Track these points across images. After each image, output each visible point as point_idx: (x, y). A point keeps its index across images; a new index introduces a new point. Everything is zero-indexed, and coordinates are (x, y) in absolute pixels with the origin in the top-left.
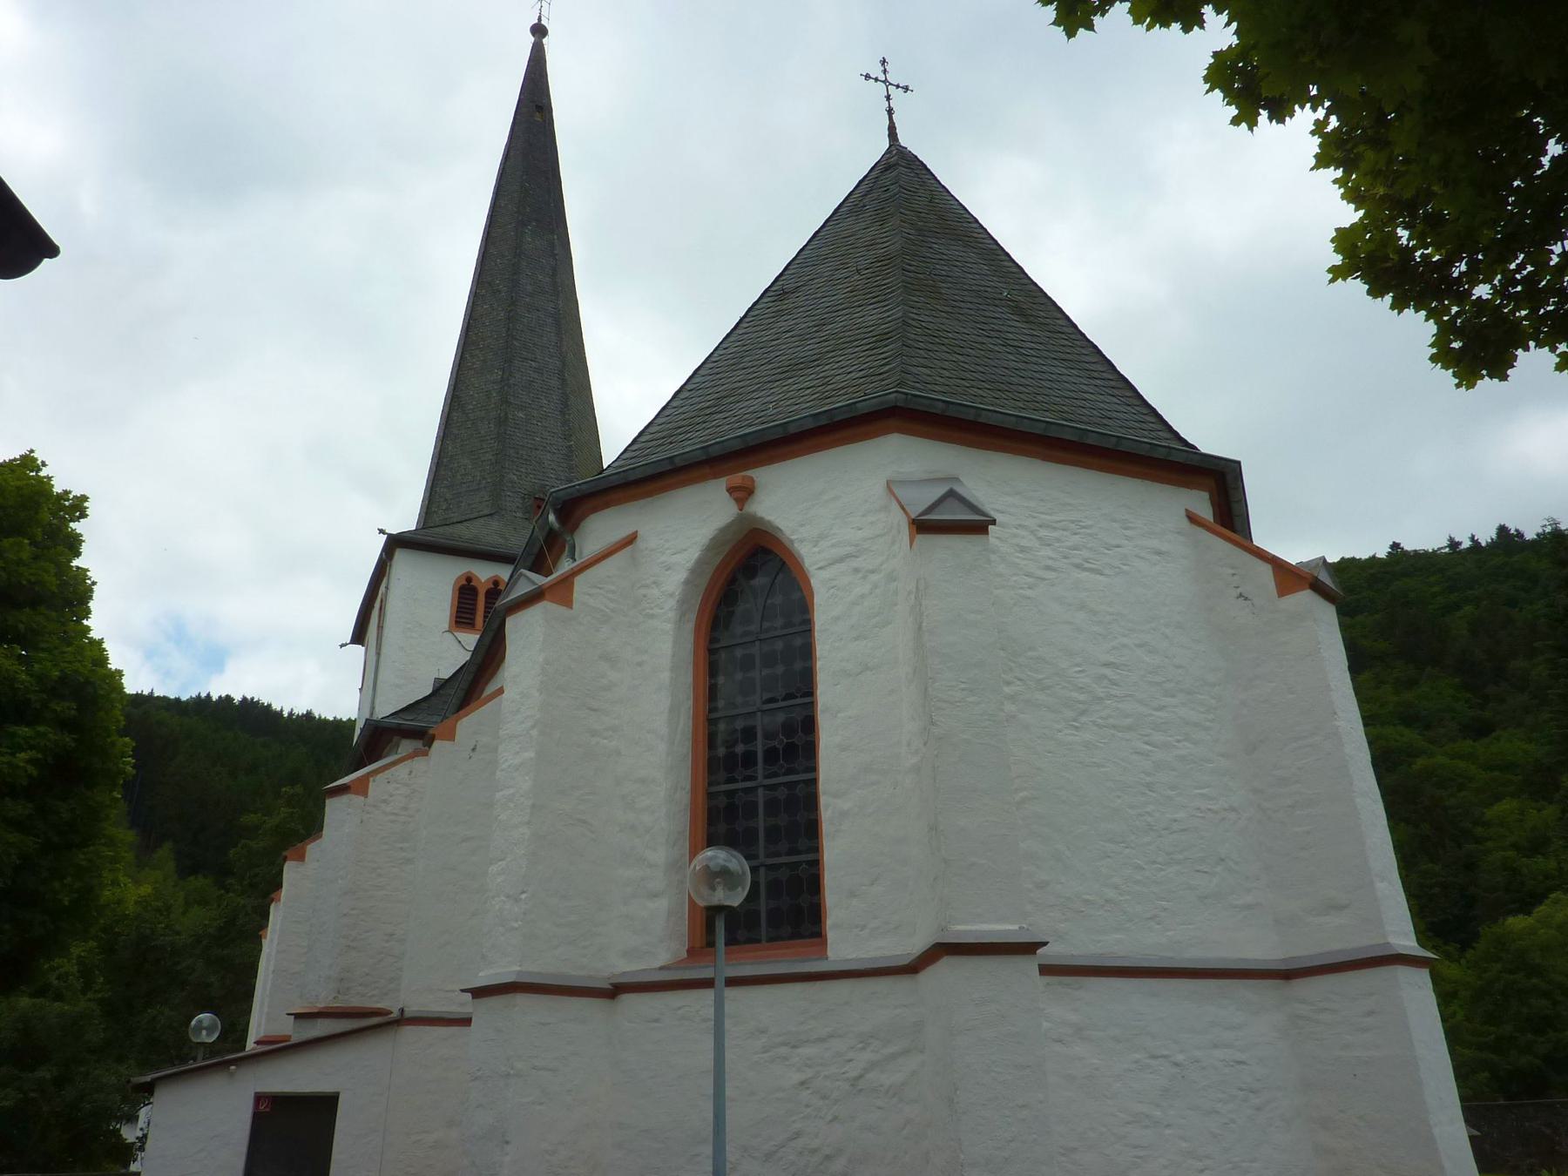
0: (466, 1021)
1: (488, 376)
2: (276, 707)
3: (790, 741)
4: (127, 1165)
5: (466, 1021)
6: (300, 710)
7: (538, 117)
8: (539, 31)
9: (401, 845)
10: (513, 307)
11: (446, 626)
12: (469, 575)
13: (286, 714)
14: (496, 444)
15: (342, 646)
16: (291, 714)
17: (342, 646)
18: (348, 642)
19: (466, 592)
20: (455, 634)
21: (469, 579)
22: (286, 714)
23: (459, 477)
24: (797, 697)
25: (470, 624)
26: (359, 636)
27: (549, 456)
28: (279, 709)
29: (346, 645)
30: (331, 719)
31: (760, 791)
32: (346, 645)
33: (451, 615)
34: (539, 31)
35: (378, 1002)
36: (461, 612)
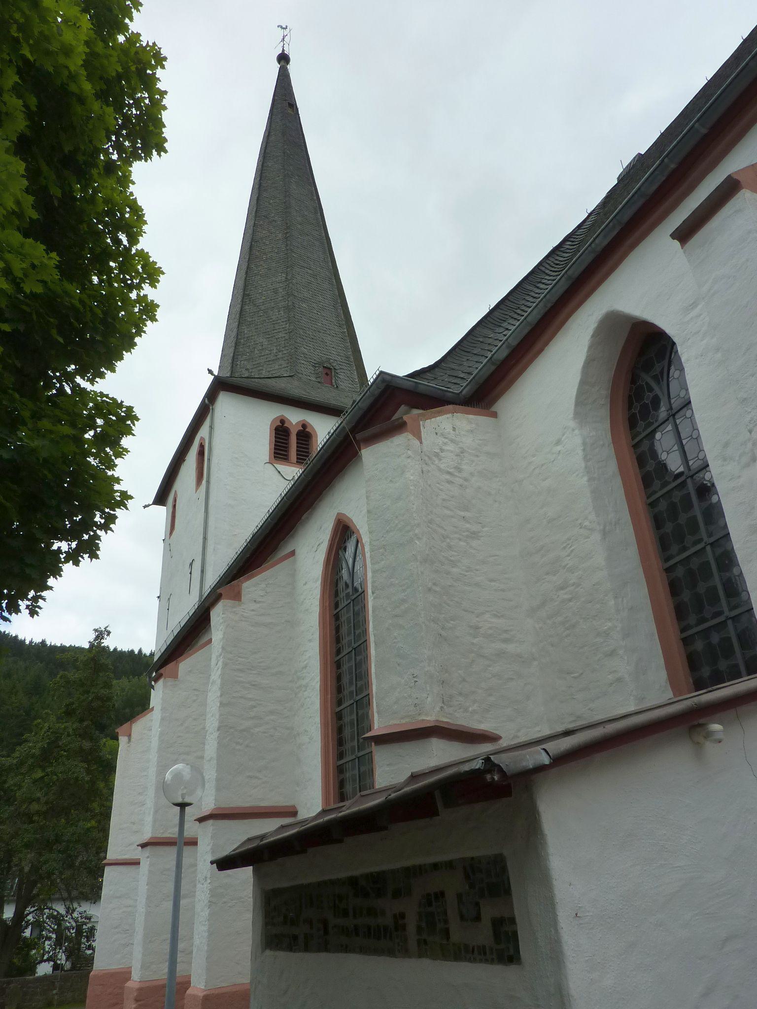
0: (136, 863)
1: (273, 279)
2: (21, 637)
3: (676, 522)
4: (33, 971)
5: (136, 863)
6: (37, 640)
7: (290, 111)
8: (283, 58)
9: (462, 514)
10: (288, 231)
11: (266, 458)
12: (283, 418)
13: (27, 642)
14: (288, 325)
15: (145, 507)
16: (31, 642)
17: (145, 507)
18: (151, 503)
19: (281, 432)
20: (275, 465)
21: (283, 421)
22: (27, 642)
23: (256, 352)
24: (657, 492)
25: (285, 459)
26: (161, 498)
27: (329, 338)
28: (23, 639)
29: (149, 505)
30: (59, 645)
31: (708, 548)
32: (149, 505)
33: (270, 449)
34: (283, 58)
35: (480, 722)
36: (279, 449)
